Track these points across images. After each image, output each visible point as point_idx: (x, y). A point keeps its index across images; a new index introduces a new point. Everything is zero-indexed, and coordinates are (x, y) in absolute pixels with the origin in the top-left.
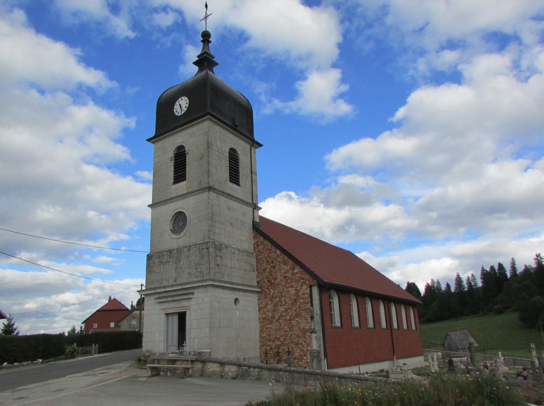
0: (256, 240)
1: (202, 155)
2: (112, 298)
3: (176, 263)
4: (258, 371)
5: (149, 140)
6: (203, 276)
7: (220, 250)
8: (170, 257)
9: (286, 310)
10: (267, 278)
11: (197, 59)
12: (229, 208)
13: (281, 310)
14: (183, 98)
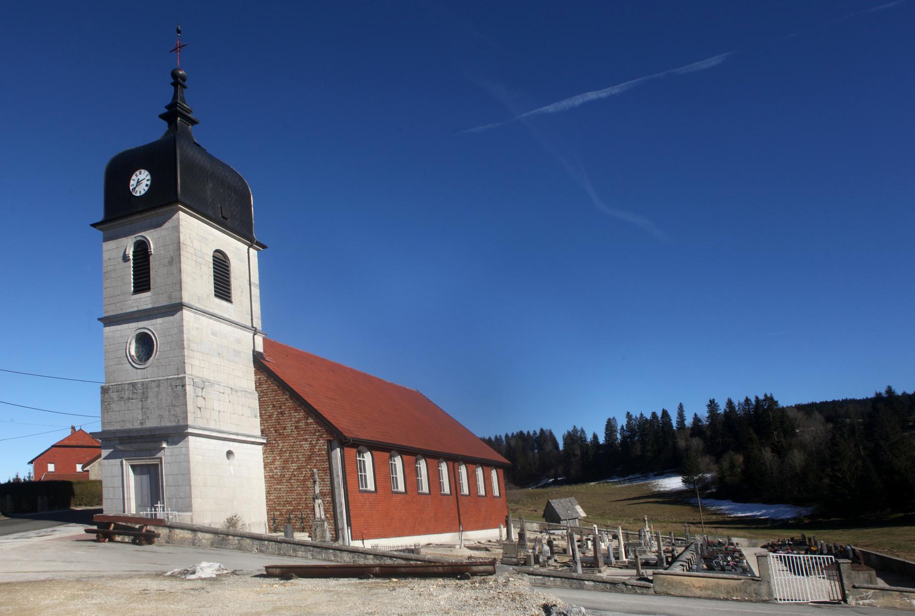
2: (77, 429)
5: (94, 225)
8: (134, 393)
9: (299, 468)
11: (166, 111)
12: (214, 334)
14: (143, 171)
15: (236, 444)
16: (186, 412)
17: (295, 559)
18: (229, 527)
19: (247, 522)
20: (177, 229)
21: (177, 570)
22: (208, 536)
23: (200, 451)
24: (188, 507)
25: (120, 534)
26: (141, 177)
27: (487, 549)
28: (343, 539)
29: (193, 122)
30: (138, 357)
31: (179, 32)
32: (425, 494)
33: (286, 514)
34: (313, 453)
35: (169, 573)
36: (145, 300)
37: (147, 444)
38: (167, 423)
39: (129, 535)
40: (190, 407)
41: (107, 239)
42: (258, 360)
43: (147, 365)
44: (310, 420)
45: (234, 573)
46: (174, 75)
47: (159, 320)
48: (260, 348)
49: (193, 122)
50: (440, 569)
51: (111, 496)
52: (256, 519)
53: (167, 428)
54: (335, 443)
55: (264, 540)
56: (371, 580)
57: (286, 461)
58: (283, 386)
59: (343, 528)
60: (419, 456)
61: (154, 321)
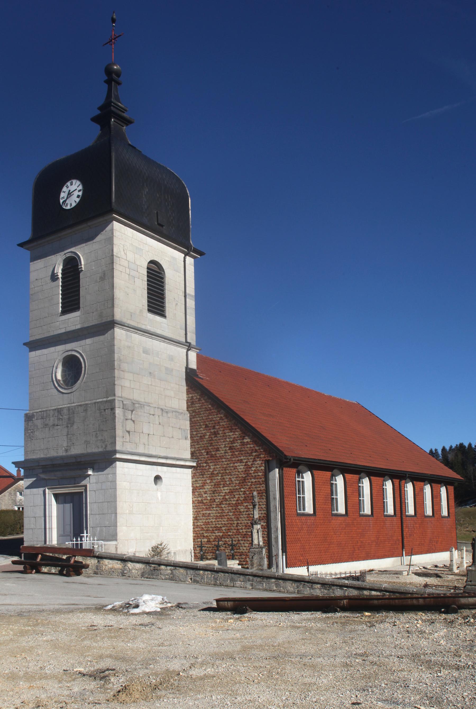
0: (190, 395)
1: (104, 274)
3: (67, 427)
4: (170, 570)
5: (21, 245)
6: (106, 446)
7: (132, 411)
8: (59, 419)
9: (231, 492)
10: (206, 449)
11: (98, 112)
12: (146, 351)
14: (74, 181)
15: (165, 468)
16: (114, 437)
17: (233, 589)
18: (153, 556)
19: (172, 550)
20: (110, 241)
21: (117, 604)
22: (138, 566)
23: (127, 475)
24: (113, 536)
25: (46, 565)
26: (72, 188)
27: (437, 576)
28: (277, 566)
29: (128, 122)
31: (113, 21)
32: (367, 516)
33: (210, 542)
34: (248, 474)
35: (110, 607)
36: (74, 321)
37: (71, 471)
38: (94, 449)
39: (56, 566)
40: (119, 432)
41: (34, 258)
42: (191, 377)
43: (74, 389)
44: (247, 440)
45: (179, 606)
46: (109, 71)
47: (88, 341)
48: (193, 365)
49: (128, 122)
50: (421, 601)
51: (32, 526)
52: (182, 548)
54: (274, 463)
55: (200, 569)
56: (338, 614)
58: (218, 404)
59: (277, 555)
60: (362, 474)
61: (82, 342)
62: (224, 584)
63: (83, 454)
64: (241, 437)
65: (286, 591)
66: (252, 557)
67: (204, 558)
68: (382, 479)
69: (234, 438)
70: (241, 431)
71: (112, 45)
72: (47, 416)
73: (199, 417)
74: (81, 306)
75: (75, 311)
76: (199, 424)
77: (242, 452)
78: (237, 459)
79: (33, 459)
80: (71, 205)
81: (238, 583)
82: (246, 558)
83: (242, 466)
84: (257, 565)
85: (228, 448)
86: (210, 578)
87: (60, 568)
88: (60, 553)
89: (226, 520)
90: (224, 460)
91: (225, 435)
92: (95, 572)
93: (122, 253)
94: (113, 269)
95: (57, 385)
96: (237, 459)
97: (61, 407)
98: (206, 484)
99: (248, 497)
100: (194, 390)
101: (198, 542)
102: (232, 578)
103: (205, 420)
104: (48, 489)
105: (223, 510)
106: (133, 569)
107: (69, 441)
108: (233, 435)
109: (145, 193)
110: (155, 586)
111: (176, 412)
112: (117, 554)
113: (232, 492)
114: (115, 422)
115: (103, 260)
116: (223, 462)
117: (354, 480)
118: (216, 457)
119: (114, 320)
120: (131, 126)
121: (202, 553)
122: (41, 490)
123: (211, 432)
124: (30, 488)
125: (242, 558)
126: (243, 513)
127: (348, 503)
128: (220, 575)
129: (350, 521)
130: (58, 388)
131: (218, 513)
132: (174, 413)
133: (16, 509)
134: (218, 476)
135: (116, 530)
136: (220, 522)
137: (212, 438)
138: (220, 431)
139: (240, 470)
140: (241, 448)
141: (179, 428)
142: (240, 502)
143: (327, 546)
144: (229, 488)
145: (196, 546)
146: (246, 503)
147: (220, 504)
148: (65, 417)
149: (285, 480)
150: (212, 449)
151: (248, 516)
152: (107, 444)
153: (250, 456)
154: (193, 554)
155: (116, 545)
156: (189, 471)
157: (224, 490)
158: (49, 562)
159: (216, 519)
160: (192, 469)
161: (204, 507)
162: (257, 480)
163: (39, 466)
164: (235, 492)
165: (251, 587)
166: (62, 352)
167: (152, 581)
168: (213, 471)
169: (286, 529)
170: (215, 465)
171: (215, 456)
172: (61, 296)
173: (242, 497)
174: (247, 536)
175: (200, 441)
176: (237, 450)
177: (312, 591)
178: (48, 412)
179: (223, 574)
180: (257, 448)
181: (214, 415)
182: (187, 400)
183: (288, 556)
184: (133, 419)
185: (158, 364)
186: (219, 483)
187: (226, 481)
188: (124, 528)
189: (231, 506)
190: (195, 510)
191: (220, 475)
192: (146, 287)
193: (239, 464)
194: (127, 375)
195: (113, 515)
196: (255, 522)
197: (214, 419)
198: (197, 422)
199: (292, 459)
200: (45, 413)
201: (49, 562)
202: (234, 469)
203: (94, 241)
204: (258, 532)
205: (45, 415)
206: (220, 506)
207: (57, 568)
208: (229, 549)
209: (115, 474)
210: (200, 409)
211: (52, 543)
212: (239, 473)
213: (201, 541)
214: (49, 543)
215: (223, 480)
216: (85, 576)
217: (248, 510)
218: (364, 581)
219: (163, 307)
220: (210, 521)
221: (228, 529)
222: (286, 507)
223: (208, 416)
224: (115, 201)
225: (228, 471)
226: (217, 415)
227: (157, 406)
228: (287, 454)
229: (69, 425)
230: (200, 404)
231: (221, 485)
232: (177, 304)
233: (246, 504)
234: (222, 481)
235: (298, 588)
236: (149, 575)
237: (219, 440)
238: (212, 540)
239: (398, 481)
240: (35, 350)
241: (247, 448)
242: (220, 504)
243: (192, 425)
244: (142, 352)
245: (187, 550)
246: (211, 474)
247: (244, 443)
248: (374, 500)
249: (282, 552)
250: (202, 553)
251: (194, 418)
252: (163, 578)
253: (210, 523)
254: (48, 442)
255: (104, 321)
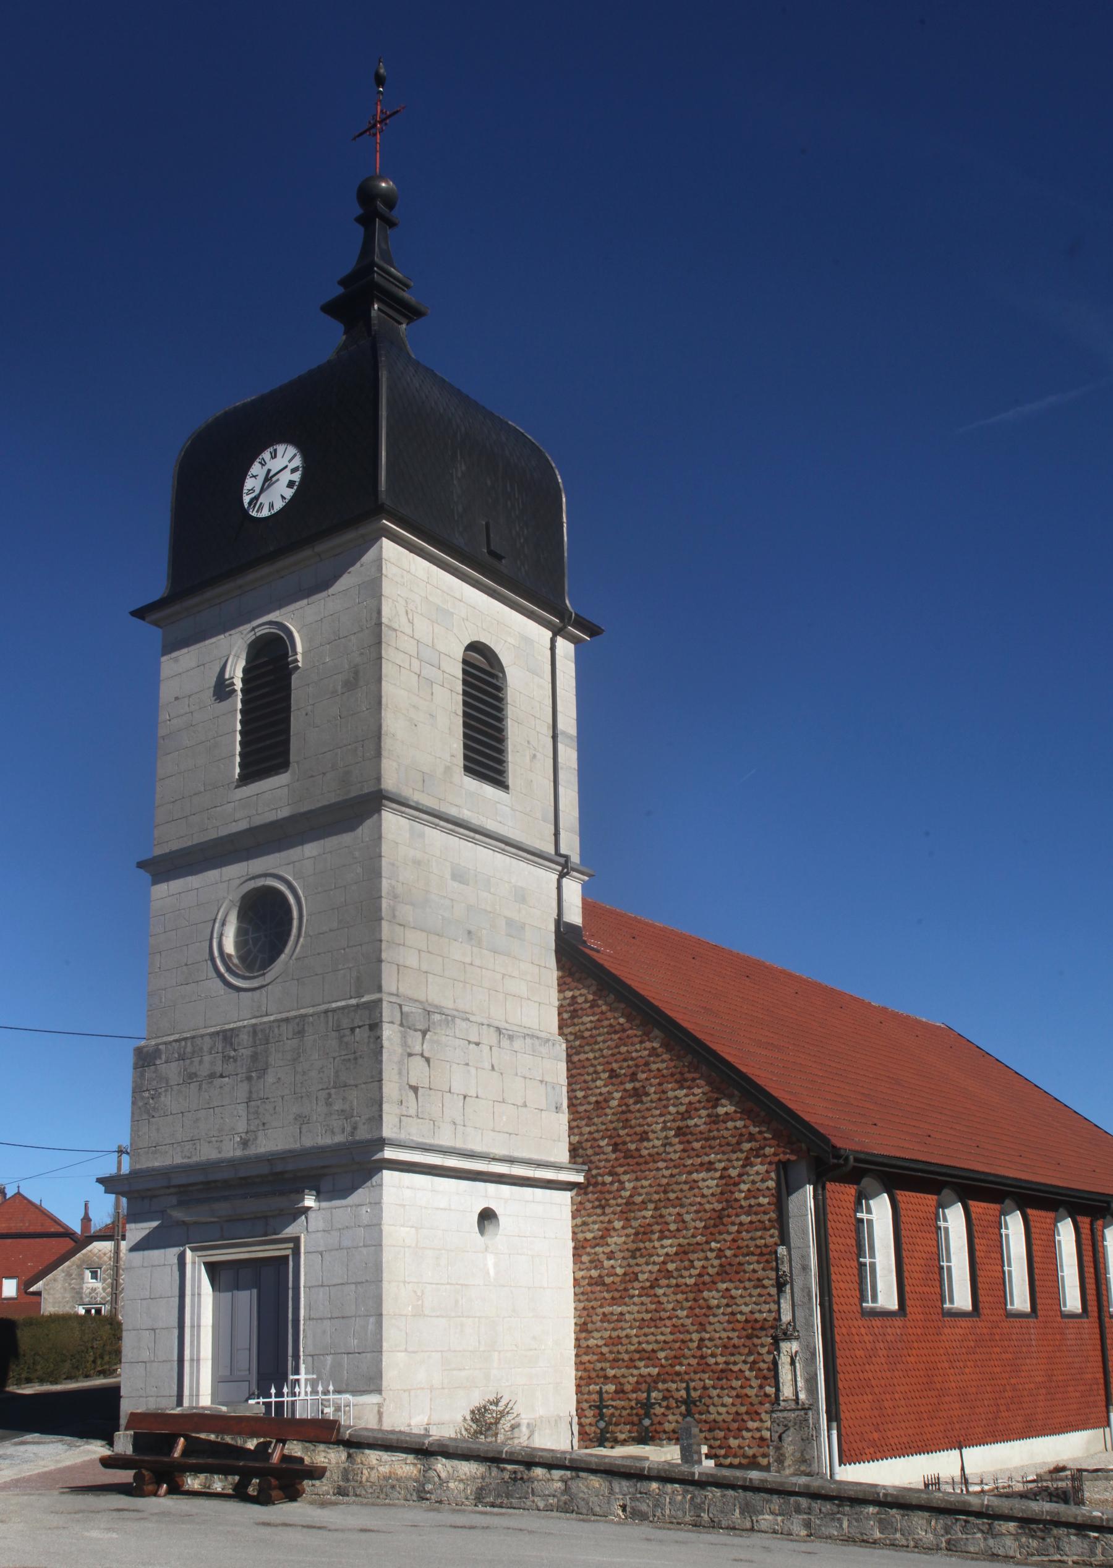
0: (569, 994)
3: (249, 1079)
4: (562, 1480)
6: (355, 1128)
7: (424, 1033)
8: (226, 1059)
9: (683, 1252)
11: (340, 290)
12: (459, 876)
13: (662, 1251)
14: (280, 448)
15: (505, 1189)
20: (373, 588)
22: (468, 1468)
25: (197, 1470)
26: (275, 465)
29: (412, 313)
30: (242, 958)
31: (380, 80)
32: (886, 1314)
34: (731, 1203)
36: (274, 797)
37: (254, 1201)
38: (319, 1137)
39: (225, 1471)
40: (391, 1088)
41: (172, 646)
44: (726, 1108)
47: (311, 849)
48: (574, 916)
49: (412, 313)
51: (145, 1355)
52: (547, 1413)
53: (321, 1151)
54: (802, 1169)
55: (649, 1478)
57: (643, 1234)
58: (646, 1015)
61: (294, 853)
62: (724, 1524)
63: (290, 1151)
64: (708, 1101)
65: (912, 1544)
66: (780, 1437)
67: (607, 1440)
68: (1051, 1214)
69: (690, 1103)
70: (709, 1083)
71: (375, 135)
72: (193, 1052)
73: (592, 1051)
74: (292, 758)
75: (277, 774)
76: (591, 1070)
77: (713, 1143)
78: (699, 1160)
79: (153, 1169)
80: (271, 506)
81: (766, 1520)
82: (725, 1438)
83: (712, 1179)
84: (795, 1462)
85: (673, 1133)
86: (681, 1502)
87: (237, 1478)
88: (240, 1433)
89: (669, 1330)
90: (661, 1165)
91: (664, 1096)
92: (339, 1487)
93: (403, 619)
94: (380, 658)
95: (222, 969)
96: (699, 1160)
97: (232, 1026)
98: (612, 1233)
99: (730, 1264)
100: (579, 980)
101: (589, 1393)
102: (747, 1504)
103: (611, 1059)
104: (193, 1250)
105: (659, 1302)
106: (451, 1477)
107: (251, 1117)
108: (686, 1095)
109: (459, 475)
110: (530, 1532)
111: (532, 1036)
112: (380, 1430)
113: (685, 1253)
114: (381, 1061)
115: (352, 637)
116: (658, 1169)
117: (990, 1218)
118: (641, 1156)
119: (380, 791)
120: (420, 323)
121: (602, 1424)
122: (172, 1253)
123: (625, 1090)
124: (144, 1249)
125: (715, 1439)
126: (715, 1311)
127: (980, 1279)
128: (710, 1495)
129: (985, 1331)
130: (226, 975)
131: (647, 1311)
132: (528, 1041)
133: (82, 1311)
134: (646, 1209)
135: (379, 1362)
136: (651, 1338)
137: (627, 1105)
138: (651, 1085)
139: (706, 1191)
140: (710, 1131)
141: (541, 1081)
142: (707, 1278)
143: (935, 1400)
144: (676, 1241)
145: (585, 1405)
146: (723, 1282)
147: (652, 1287)
148: (244, 1054)
149: (830, 1216)
150: (627, 1135)
151: (732, 1318)
152: (356, 1123)
153: (734, 1152)
154: (576, 1428)
155: (380, 1405)
156: (565, 1198)
157: (663, 1247)
158: (210, 1461)
159: (640, 1328)
160: (574, 1192)
161: (606, 1295)
162: (754, 1218)
163: (168, 1187)
164: (694, 1252)
165: (804, 1533)
166: (238, 882)
167: (510, 1515)
168: (631, 1196)
169: (838, 1353)
170: (637, 1179)
171: (636, 1154)
172: (239, 738)
173: (713, 1266)
174: (729, 1374)
175: (594, 1114)
176: (699, 1136)
177: (991, 1542)
178: (199, 1041)
179: (718, 1492)
180: (754, 1130)
181: (633, 1044)
182: (561, 1006)
183: (843, 1431)
184: (426, 1054)
185: (489, 909)
186: (649, 1229)
187: (667, 1223)
188: (401, 1356)
189: (683, 1293)
190: (582, 1305)
191: (651, 1206)
192: (460, 709)
193: (703, 1175)
194: (414, 938)
195: (372, 1320)
196: (785, 1334)
197: (634, 1055)
198: (587, 1064)
199: (851, 1157)
200: (189, 1044)
201: (210, 1461)
202: (691, 1188)
203: (331, 591)
204: (793, 1363)
205: (189, 1049)
206: (652, 1292)
207: (230, 1478)
208: (677, 1411)
209: (377, 1204)
210: (595, 1028)
211: (198, 1401)
212: (704, 1201)
213: (600, 1393)
214: (191, 1401)
215: (660, 1220)
216: (311, 1503)
217: (731, 1302)
218: (1080, 1502)
219: (502, 762)
220: (624, 1333)
221: (675, 1357)
222: (834, 1292)
223: (617, 1047)
224: (387, 490)
225: (672, 1196)
226: (641, 1042)
227: (485, 1022)
228: (839, 1145)
229: (254, 1074)
230: (593, 1014)
231: (652, 1232)
232: (534, 756)
233: (724, 1286)
234: (657, 1223)
235: (947, 1533)
236: (499, 1496)
237: (648, 1109)
238: (628, 1387)
239: (1087, 1220)
240: (167, 880)
241: (727, 1129)
242: (652, 1287)
243: (574, 1072)
244: (448, 876)
245: (560, 1418)
246: (627, 1204)
247: (718, 1116)
248: (1036, 1271)
249: (829, 1420)
250: (602, 1424)
251: (578, 1053)
252: (541, 1505)
253: (624, 1341)
254: (197, 1120)
255: (353, 795)
